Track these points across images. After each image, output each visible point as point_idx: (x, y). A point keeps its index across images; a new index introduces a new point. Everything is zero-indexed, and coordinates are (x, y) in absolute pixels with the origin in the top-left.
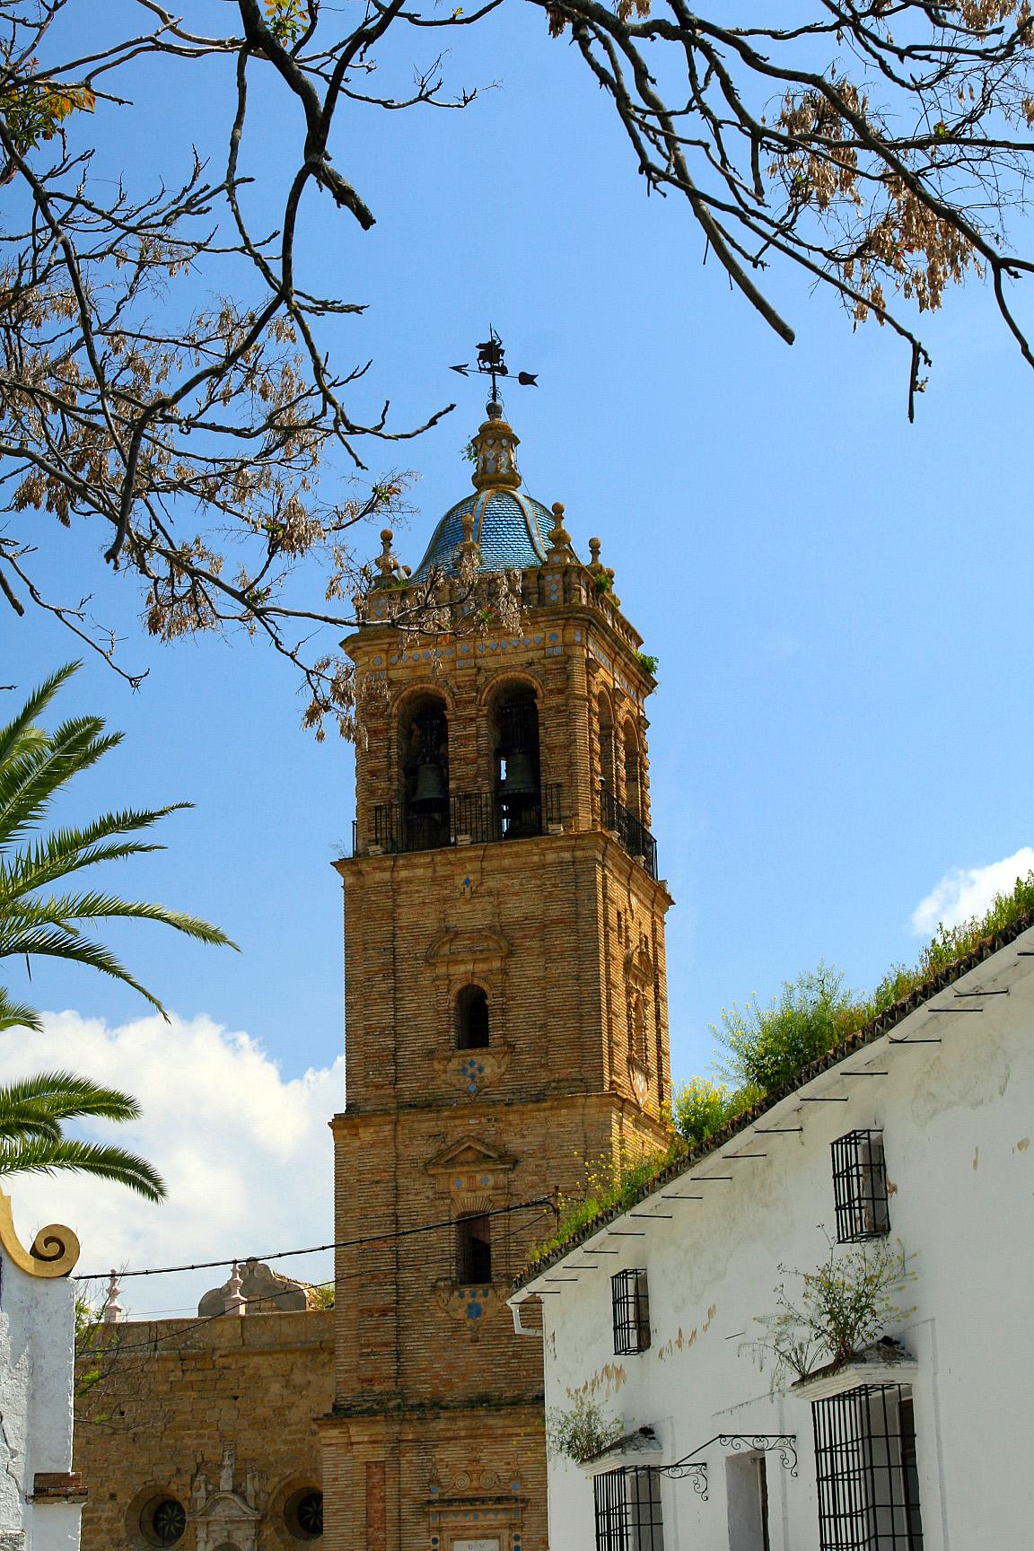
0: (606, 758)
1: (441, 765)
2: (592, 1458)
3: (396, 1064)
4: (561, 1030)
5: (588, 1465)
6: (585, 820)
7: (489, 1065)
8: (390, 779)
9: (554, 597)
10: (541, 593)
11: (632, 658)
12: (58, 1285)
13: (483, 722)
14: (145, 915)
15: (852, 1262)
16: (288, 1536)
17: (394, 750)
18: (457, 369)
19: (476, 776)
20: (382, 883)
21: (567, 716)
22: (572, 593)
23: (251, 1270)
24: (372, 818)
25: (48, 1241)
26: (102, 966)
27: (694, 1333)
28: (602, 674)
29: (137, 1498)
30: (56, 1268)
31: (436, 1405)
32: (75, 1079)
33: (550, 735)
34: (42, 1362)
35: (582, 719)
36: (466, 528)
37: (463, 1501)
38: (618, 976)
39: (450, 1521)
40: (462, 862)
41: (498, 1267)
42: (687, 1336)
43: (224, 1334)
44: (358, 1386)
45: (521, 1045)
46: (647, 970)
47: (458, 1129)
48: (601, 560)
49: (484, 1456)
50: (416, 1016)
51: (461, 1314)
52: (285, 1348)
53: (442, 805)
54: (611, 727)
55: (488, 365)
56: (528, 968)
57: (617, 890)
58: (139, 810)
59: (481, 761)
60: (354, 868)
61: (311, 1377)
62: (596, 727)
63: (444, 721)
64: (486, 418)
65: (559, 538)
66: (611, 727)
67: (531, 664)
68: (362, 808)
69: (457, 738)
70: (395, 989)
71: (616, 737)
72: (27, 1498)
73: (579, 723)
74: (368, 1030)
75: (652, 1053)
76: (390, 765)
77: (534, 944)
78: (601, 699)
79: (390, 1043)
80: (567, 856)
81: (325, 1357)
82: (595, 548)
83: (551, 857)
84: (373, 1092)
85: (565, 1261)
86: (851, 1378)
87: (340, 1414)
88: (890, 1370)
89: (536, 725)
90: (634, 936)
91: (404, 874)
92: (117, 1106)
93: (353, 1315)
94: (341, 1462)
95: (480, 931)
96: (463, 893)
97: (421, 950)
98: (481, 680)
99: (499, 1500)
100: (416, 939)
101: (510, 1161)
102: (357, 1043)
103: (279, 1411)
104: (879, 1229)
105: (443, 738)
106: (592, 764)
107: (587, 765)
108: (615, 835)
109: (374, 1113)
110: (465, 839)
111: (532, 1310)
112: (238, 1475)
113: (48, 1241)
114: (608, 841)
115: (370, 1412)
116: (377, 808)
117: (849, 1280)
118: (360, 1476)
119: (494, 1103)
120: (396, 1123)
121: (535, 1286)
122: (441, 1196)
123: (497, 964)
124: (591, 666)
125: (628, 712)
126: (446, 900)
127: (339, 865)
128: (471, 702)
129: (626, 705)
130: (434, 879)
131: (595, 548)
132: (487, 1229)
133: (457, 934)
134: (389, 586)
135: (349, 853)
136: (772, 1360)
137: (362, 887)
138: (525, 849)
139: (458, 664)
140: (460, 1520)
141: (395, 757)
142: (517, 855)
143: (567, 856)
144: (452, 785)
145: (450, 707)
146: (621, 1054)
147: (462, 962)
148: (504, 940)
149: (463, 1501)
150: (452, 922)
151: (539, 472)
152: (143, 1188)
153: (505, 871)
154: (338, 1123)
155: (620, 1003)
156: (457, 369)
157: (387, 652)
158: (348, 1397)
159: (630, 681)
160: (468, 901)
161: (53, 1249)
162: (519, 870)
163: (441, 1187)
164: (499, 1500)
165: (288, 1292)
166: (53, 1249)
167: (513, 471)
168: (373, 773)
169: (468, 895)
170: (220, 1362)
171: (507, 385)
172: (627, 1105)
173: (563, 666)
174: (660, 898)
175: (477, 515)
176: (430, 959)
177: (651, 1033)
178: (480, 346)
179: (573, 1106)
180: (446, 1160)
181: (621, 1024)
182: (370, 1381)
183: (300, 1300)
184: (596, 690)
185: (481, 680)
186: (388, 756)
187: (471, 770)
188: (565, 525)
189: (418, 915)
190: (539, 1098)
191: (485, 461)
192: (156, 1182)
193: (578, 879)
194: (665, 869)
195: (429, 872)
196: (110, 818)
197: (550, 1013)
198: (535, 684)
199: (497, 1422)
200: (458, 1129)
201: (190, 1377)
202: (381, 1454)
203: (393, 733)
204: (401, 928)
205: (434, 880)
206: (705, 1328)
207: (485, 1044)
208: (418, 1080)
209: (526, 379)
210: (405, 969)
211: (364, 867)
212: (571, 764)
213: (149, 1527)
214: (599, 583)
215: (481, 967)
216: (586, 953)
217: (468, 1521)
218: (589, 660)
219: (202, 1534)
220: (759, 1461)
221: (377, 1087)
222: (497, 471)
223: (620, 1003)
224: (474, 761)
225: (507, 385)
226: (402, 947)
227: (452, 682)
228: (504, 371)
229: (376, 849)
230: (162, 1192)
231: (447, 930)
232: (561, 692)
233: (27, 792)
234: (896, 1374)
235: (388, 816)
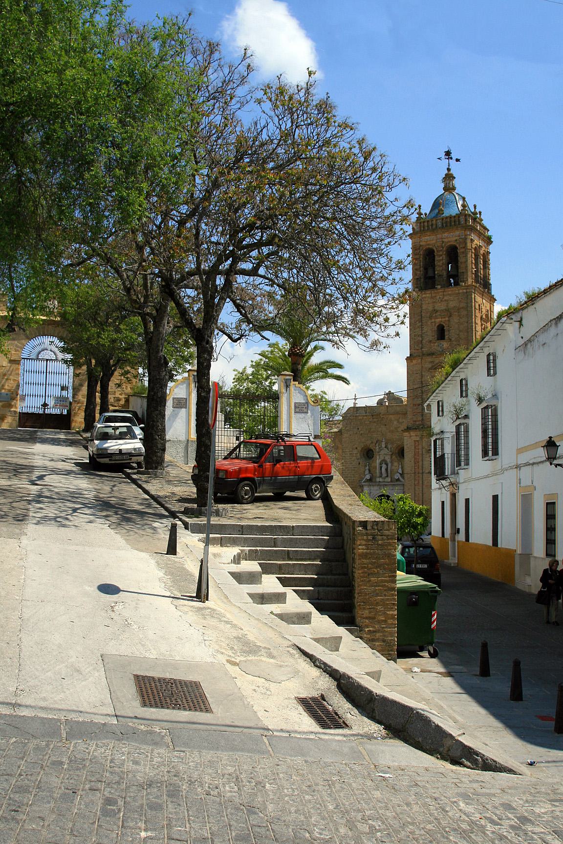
0: (476, 265)
1: (433, 266)
7: (445, 344)
22: (469, 221)
23: (389, 394)
33: (461, 259)
35: (469, 256)
38: (478, 321)
43: (382, 410)
52: (398, 413)
56: (455, 320)
82: (475, 207)
87: (408, 429)
90: (484, 311)
92: (340, 366)
97: (428, 315)
103: (396, 428)
110: (439, 287)
112: (386, 444)
117: (458, 405)
124: (472, 241)
129: (483, 248)
131: (475, 207)
148: (449, 312)
154: (407, 359)
155: (479, 328)
158: (410, 425)
165: (399, 400)
176: (430, 318)
193: (468, 297)
194: (494, 292)
202: (418, 439)
205: (432, 297)
209: (458, 160)
210: (424, 320)
212: (467, 267)
214: (475, 217)
216: (469, 315)
225: (453, 162)
226: (423, 315)
234: (466, 421)
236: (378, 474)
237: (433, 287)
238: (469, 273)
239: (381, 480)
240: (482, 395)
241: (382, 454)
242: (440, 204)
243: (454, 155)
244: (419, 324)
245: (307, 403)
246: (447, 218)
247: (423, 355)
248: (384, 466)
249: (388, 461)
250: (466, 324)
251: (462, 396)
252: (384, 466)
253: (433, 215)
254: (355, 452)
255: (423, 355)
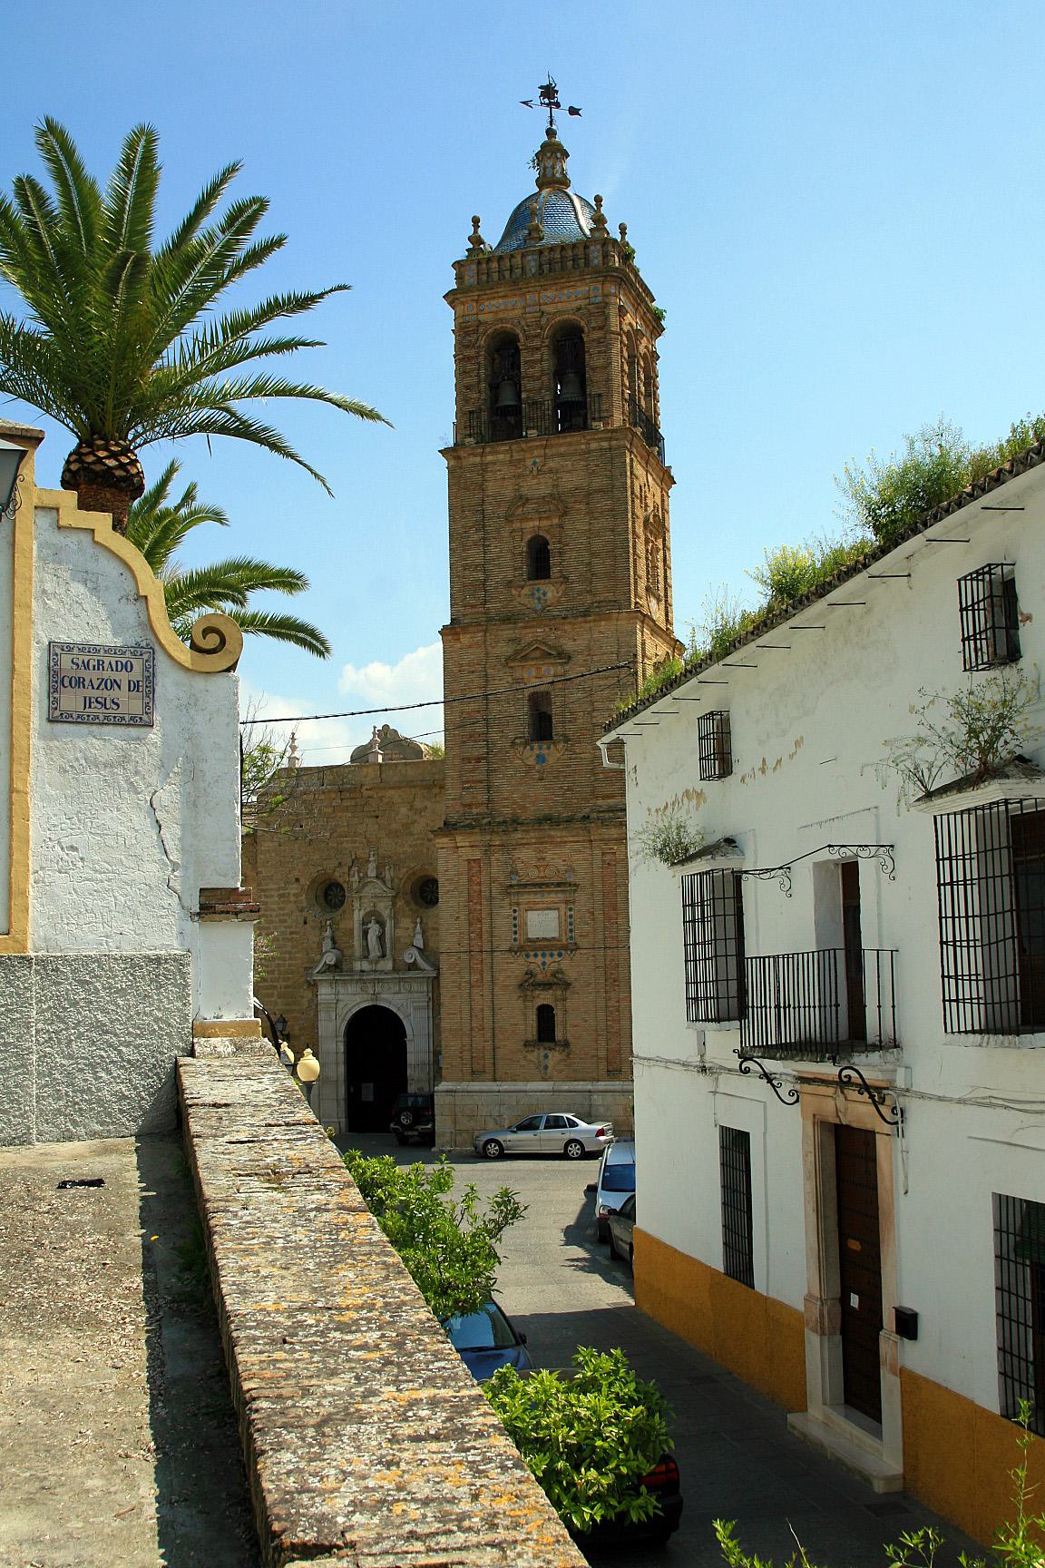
2: (682, 862)
4: (600, 566)
5: (679, 867)
6: (618, 419)
7: (550, 591)
10: (587, 258)
11: (649, 309)
12: (221, 680)
13: (545, 350)
14: (309, 396)
15: (988, 685)
16: (414, 907)
20: (474, 465)
22: (605, 261)
24: (467, 421)
25: (206, 632)
26: (275, 447)
27: (779, 762)
28: (628, 318)
29: (313, 882)
30: (219, 661)
31: (515, 822)
32: (254, 562)
33: (593, 359)
34: (204, 766)
35: (616, 349)
36: (533, 213)
37: (535, 885)
38: (640, 530)
39: (524, 898)
41: (557, 729)
42: (771, 763)
43: (369, 776)
44: (461, 810)
45: (573, 577)
46: (658, 527)
47: (528, 636)
48: (627, 238)
49: (548, 856)
51: (531, 761)
52: (410, 784)
53: (516, 410)
56: (577, 524)
57: (639, 471)
58: (302, 291)
61: (428, 804)
63: (518, 351)
65: (599, 220)
72: (192, 915)
75: (661, 586)
77: (582, 506)
78: (628, 334)
79: (481, 576)
80: (605, 444)
81: (436, 790)
82: (623, 229)
83: (594, 445)
84: (470, 610)
85: (653, 708)
86: (991, 792)
87: (449, 828)
88: (1031, 785)
91: (490, 458)
92: (288, 581)
93: (457, 762)
94: (450, 861)
97: (502, 511)
98: (544, 321)
99: (559, 885)
101: (565, 657)
103: (406, 826)
104: (1012, 654)
107: (619, 379)
108: (639, 430)
109: (470, 624)
110: (533, 433)
111: (618, 744)
113: (206, 632)
114: (634, 434)
115: (470, 826)
118: (463, 868)
119: (554, 618)
120: (485, 631)
121: (621, 730)
122: (517, 681)
123: (556, 521)
124: (622, 311)
126: (519, 476)
131: (623, 229)
132: (549, 704)
135: (451, 444)
136: (895, 779)
138: (576, 441)
140: (532, 898)
142: (570, 444)
143: (605, 444)
144: (524, 395)
146: (642, 584)
148: (559, 504)
149: (535, 885)
150: (524, 491)
151: (584, 178)
152: (312, 648)
153: (561, 455)
154: (445, 632)
155: (641, 548)
158: (454, 817)
161: (213, 640)
162: (572, 454)
163: (517, 675)
164: (559, 885)
166: (213, 640)
168: (467, 388)
170: (366, 793)
171: (561, 115)
172: (646, 618)
174: (667, 479)
176: (509, 519)
177: (661, 572)
179: (609, 619)
180: (521, 656)
181: (642, 563)
182: (470, 805)
183: (417, 751)
184: (626, 328)
187: (537, 384)
188: (603, 210)
189: (499, 486)
190: (586, 614)
192: (323, 643)
195: (508, 457)
196: (276, 299)
197: (593, 554)
199: (557, 834)
200: (528, 636)
201: (346, 803)
202: (477, 854)
203: (481, 359)
206: (791, 757)
207: (548, 577)
209: (574, 111)
211: (462, 453)
212: (608, 380)
213: (322, 900)
214: (627, 256)
215: (545, 523)
216: (618, 512)
217: (538, 898)
219: (356, 904)
220: (850, 872)
223: (641, 548)
224: (539, 378)
225: (561, 115)
226: (489, 509)
228: (558, 105)
230: (327, 649)
232: (601, 328)
233: (202, 274)
236: (358, 951)
238: (616, 398)
239: (366, 966)
241: (369, 896)
245: (148, 650)
246: (552, 249)
247: (490, 620)
248: (374, 930)
249: (386, 913)
250: (609, 536)
252: (374, 930)
254: (294, 889)
255: (490, 620)
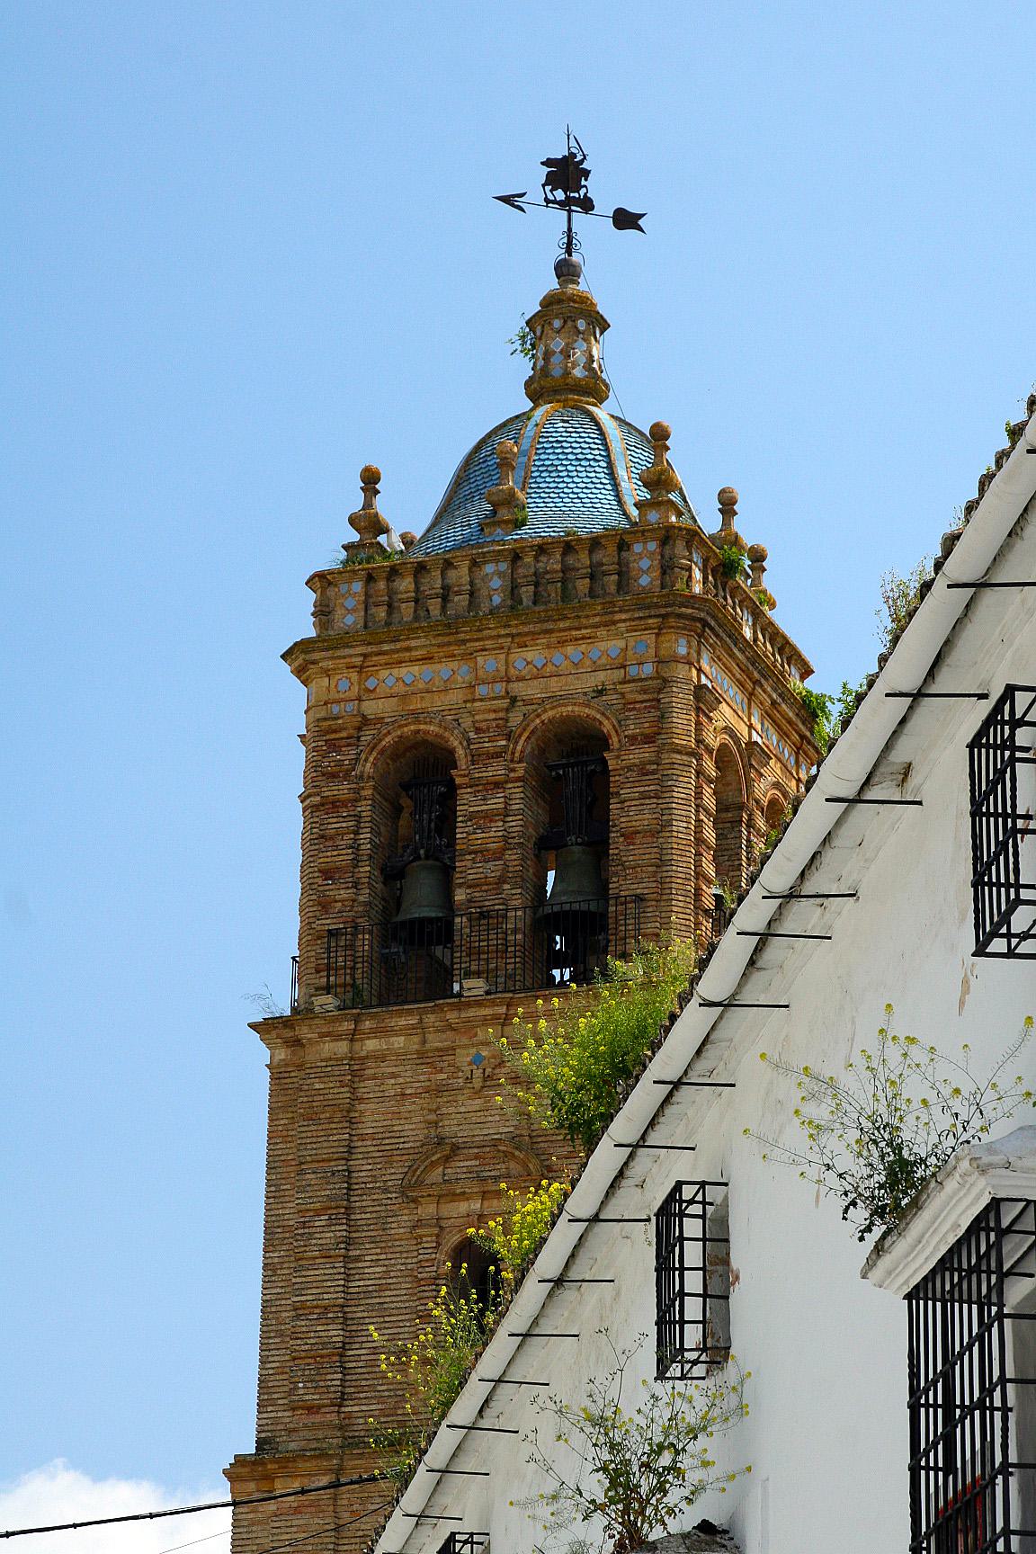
3: (345, 1371)
8: (356, 885)
9: (644, 581)
11: (786, 695)
13: (516, 791)
17: (365, 835)
18: (507, 200)
19: (502, 880)
20: (335, 1060)
21: (657, 779)
24: (324, 953)
33: (628, 812)
35: (684, 786)
36: (506, 464)
40: (469, 1028)
48: (738, 525)
50: (382, 1288)
53: (441, 930)
54: (741, 807)
55: (560, 195)
59: (512, 857)
60: (288, 1033)
62: (709, 801)
63: (452, 788)
64: (552, 283)
65: (659, 482)
66: (741, 807)
67: (600, 692)
68: (309, 934)
69: (471, 817)
70: (349, 1242)
71: (751, 824)
73: (679, 793)
74: (299, 1310)
76: (356, 862)
78: (723, 757)
79: (335, 1333)
82: (727, 505)
89: (607, 796)
91: (371, 1045)
95: (495, 1143)
96: (469, 1080)
97: (394, 1174)
98: (515, 719)
100: (389, 1160)
102: (281, 1334)
105: (446, 822)
106: (698, 865)
109: (300, 1455)
110: (476, 986)
116: (332, 934)
124: (704, 700)
125: (777, 785)
126: (439, 1090)
127: (264, 1028)
128: (497, 755)
130: (421, 1054)
131: (727, 505)
133: (455, 1148)
134: (369, 559)
137: (300, 1067)
139: (482, 690)
141: (366, 847)
144: (460, 896)
145: (462, 763)
147: (464, 1196)
150: (450, 1128)
154: (239, 1470)
156: (507, 200)
157: (361, 669)
159: (783, 734)
160: (478, 1093)
167: (594, 375)
168: (327, 874)
169: (477, 1083)
173: (656, 692)
175: (525, 443)
176: (410, 1192)
178: (548, 163)
185: (515, 719)
186: (356, 847)
187: (492, 869)
189: (391, 1114)
191: (548, 355)
195: (414, 1043)
198: (607, 727)
203: (365, 808)
204: (362, 1137)
205: (423, 1057)
208: (380, 1400)
209: (625, 220)
211: (305, 1032)
212: (662, 863)
214: (731, 564)
218: (700, 688)
221: (311, 1409)
222: (567, 373)
225: (593, 230)
226: (363, 1170)
227: (467, 722)
228: (587, 205)
229: (327, 1002)
231: (441, 1141)
232: (649, 739)
235: (352, 947)
237: (437, 987)
240: (918, 1140)
242: (506, 464)
243: (604, 189)
244: (327, 1235)
246: (542, 549)
251: (668, 1354)
253: (455, 533)
